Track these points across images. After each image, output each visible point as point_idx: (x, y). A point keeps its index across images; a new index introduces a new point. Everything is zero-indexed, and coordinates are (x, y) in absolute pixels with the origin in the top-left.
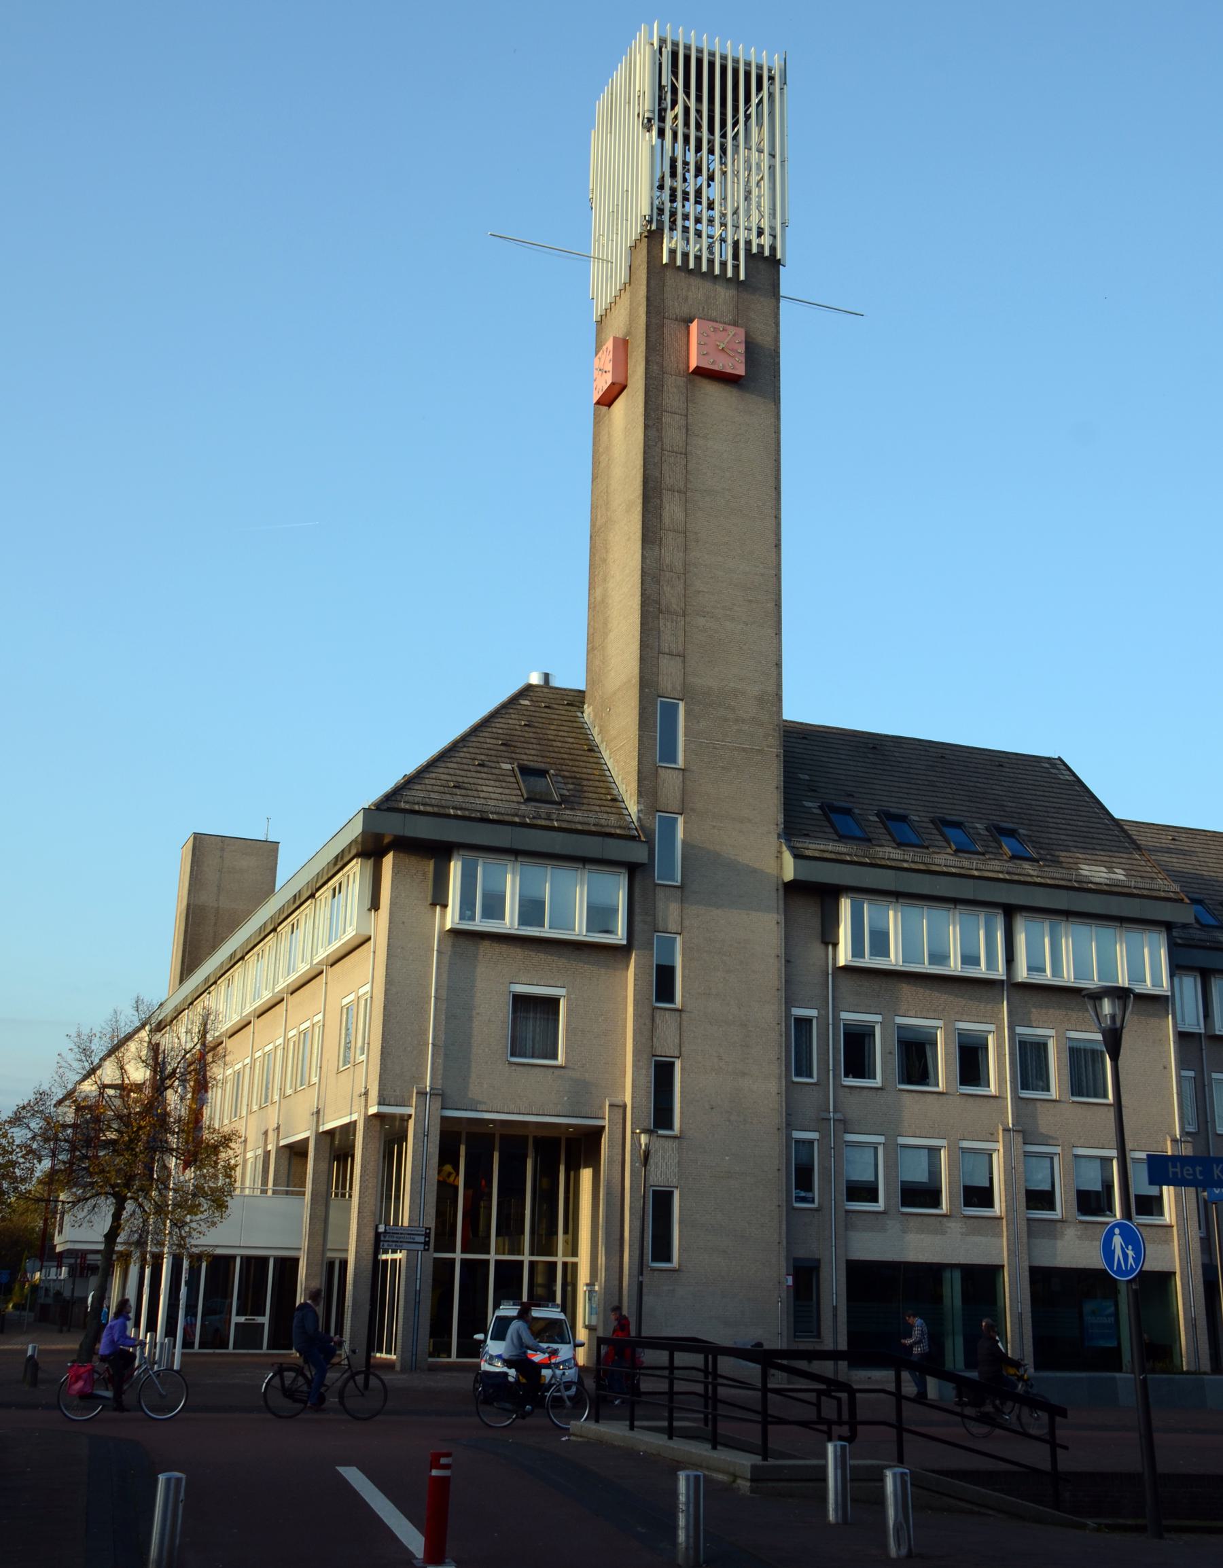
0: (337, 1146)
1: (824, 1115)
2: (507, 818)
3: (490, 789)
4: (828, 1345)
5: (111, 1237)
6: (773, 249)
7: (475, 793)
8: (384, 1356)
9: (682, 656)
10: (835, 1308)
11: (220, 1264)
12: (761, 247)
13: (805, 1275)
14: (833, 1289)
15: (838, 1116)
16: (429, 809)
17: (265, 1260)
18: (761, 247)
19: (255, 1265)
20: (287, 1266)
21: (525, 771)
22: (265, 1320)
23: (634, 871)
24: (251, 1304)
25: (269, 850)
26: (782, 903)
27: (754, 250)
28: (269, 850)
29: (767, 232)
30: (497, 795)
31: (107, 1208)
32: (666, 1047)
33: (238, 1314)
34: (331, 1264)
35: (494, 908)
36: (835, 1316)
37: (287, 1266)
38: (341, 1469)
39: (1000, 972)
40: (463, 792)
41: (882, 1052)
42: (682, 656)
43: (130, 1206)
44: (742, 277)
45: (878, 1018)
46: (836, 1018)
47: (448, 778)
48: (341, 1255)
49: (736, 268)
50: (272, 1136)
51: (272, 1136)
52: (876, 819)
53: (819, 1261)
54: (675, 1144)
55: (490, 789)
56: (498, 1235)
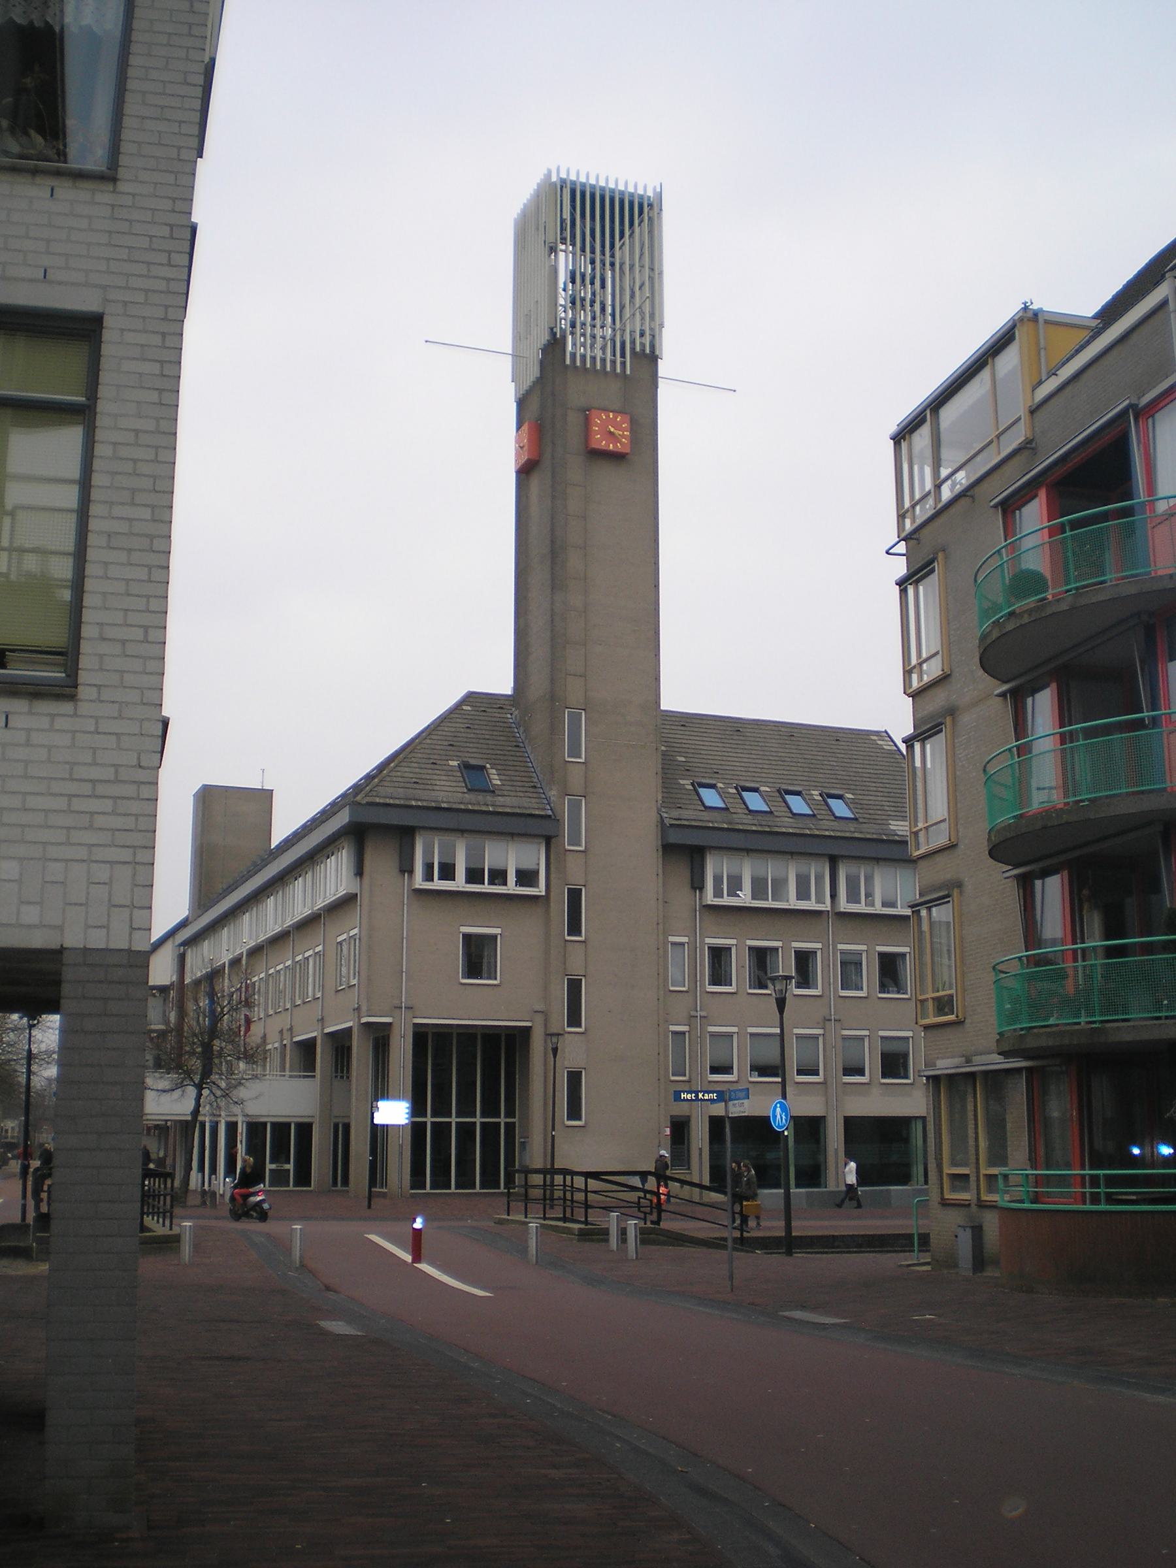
0: (340, 1044)
1: (693, 1013)
2: (454, 806)
3: (443, 783)
4: (696, 1180)
5: (196, 1112)
6: (653, 346)
7: (430, 787)
8: (377, 1190)
9: (584, 676)
10: (701, 1149)
11: (256, 1129)
12: (643, 345)
13: (680, 1129)
14: (700, 1136)
15: (703, 1014)
16: (397, 802)
17: (288, 1125)
18: (643, 345)
19: (281, 1129)
20: (305, 1130)
21: (467, 766)
22: (290, 1167)
23: (548, 840)
24: (280, 1153)
25: (264, 798)
26: (660, 860)
27: (638, 349)
28: (264, 798)
29: (648, 332)
30: (447, 790)
31: (192, 1091)
32: (576, 966)
33: (271, 1163)
34: (336, 1126)
35: (448, 872)
36: (701, 1154)
37: (305, 1130)
38: (323, 1324)
39: (827, 906)
40: (422, 786)
41: (739, 966)
42: (584, 676)
43: (205, 1092)
44: (628, 372)
45: (734, 942)
46: (702, 942)
47: (411, 775)
48: (346, 1121)
49: (623, 364)
50: (286, 1035)
51: (286, 1035)
52: (734, 791)
53: (689, 1117)
54: (582, 1038)
55: (443, 783)
56: (733, 1141)
